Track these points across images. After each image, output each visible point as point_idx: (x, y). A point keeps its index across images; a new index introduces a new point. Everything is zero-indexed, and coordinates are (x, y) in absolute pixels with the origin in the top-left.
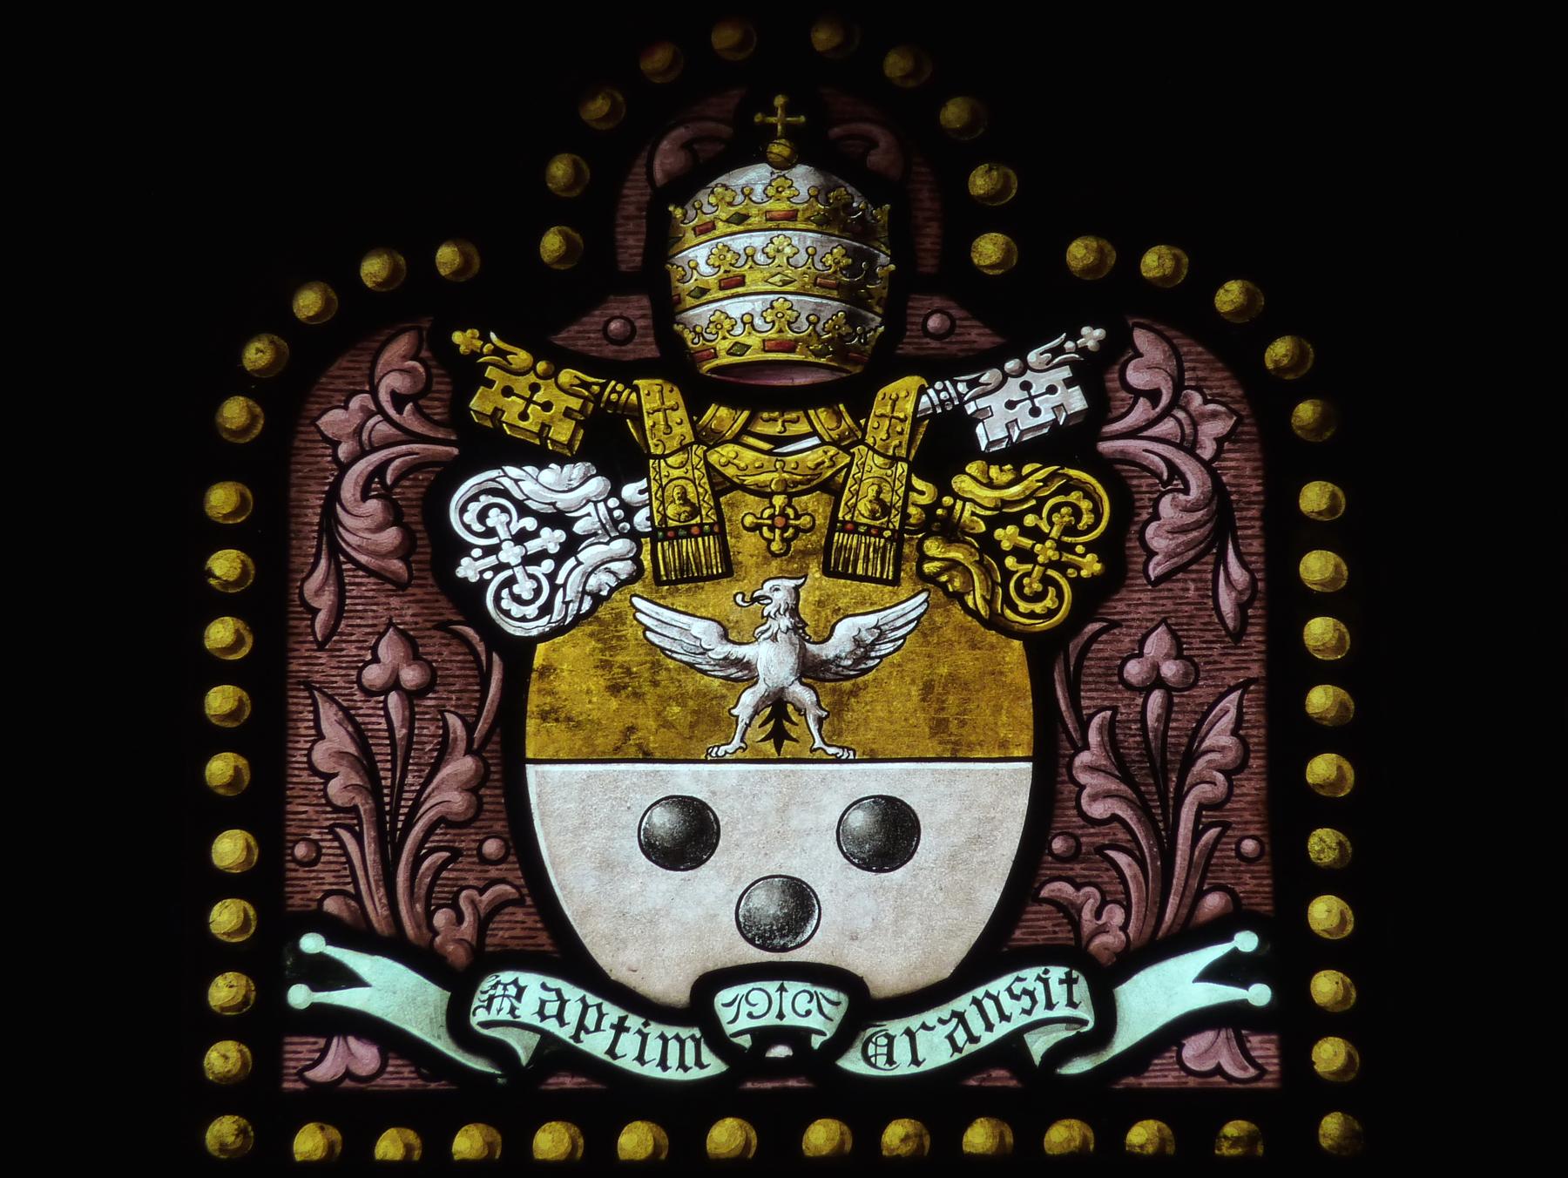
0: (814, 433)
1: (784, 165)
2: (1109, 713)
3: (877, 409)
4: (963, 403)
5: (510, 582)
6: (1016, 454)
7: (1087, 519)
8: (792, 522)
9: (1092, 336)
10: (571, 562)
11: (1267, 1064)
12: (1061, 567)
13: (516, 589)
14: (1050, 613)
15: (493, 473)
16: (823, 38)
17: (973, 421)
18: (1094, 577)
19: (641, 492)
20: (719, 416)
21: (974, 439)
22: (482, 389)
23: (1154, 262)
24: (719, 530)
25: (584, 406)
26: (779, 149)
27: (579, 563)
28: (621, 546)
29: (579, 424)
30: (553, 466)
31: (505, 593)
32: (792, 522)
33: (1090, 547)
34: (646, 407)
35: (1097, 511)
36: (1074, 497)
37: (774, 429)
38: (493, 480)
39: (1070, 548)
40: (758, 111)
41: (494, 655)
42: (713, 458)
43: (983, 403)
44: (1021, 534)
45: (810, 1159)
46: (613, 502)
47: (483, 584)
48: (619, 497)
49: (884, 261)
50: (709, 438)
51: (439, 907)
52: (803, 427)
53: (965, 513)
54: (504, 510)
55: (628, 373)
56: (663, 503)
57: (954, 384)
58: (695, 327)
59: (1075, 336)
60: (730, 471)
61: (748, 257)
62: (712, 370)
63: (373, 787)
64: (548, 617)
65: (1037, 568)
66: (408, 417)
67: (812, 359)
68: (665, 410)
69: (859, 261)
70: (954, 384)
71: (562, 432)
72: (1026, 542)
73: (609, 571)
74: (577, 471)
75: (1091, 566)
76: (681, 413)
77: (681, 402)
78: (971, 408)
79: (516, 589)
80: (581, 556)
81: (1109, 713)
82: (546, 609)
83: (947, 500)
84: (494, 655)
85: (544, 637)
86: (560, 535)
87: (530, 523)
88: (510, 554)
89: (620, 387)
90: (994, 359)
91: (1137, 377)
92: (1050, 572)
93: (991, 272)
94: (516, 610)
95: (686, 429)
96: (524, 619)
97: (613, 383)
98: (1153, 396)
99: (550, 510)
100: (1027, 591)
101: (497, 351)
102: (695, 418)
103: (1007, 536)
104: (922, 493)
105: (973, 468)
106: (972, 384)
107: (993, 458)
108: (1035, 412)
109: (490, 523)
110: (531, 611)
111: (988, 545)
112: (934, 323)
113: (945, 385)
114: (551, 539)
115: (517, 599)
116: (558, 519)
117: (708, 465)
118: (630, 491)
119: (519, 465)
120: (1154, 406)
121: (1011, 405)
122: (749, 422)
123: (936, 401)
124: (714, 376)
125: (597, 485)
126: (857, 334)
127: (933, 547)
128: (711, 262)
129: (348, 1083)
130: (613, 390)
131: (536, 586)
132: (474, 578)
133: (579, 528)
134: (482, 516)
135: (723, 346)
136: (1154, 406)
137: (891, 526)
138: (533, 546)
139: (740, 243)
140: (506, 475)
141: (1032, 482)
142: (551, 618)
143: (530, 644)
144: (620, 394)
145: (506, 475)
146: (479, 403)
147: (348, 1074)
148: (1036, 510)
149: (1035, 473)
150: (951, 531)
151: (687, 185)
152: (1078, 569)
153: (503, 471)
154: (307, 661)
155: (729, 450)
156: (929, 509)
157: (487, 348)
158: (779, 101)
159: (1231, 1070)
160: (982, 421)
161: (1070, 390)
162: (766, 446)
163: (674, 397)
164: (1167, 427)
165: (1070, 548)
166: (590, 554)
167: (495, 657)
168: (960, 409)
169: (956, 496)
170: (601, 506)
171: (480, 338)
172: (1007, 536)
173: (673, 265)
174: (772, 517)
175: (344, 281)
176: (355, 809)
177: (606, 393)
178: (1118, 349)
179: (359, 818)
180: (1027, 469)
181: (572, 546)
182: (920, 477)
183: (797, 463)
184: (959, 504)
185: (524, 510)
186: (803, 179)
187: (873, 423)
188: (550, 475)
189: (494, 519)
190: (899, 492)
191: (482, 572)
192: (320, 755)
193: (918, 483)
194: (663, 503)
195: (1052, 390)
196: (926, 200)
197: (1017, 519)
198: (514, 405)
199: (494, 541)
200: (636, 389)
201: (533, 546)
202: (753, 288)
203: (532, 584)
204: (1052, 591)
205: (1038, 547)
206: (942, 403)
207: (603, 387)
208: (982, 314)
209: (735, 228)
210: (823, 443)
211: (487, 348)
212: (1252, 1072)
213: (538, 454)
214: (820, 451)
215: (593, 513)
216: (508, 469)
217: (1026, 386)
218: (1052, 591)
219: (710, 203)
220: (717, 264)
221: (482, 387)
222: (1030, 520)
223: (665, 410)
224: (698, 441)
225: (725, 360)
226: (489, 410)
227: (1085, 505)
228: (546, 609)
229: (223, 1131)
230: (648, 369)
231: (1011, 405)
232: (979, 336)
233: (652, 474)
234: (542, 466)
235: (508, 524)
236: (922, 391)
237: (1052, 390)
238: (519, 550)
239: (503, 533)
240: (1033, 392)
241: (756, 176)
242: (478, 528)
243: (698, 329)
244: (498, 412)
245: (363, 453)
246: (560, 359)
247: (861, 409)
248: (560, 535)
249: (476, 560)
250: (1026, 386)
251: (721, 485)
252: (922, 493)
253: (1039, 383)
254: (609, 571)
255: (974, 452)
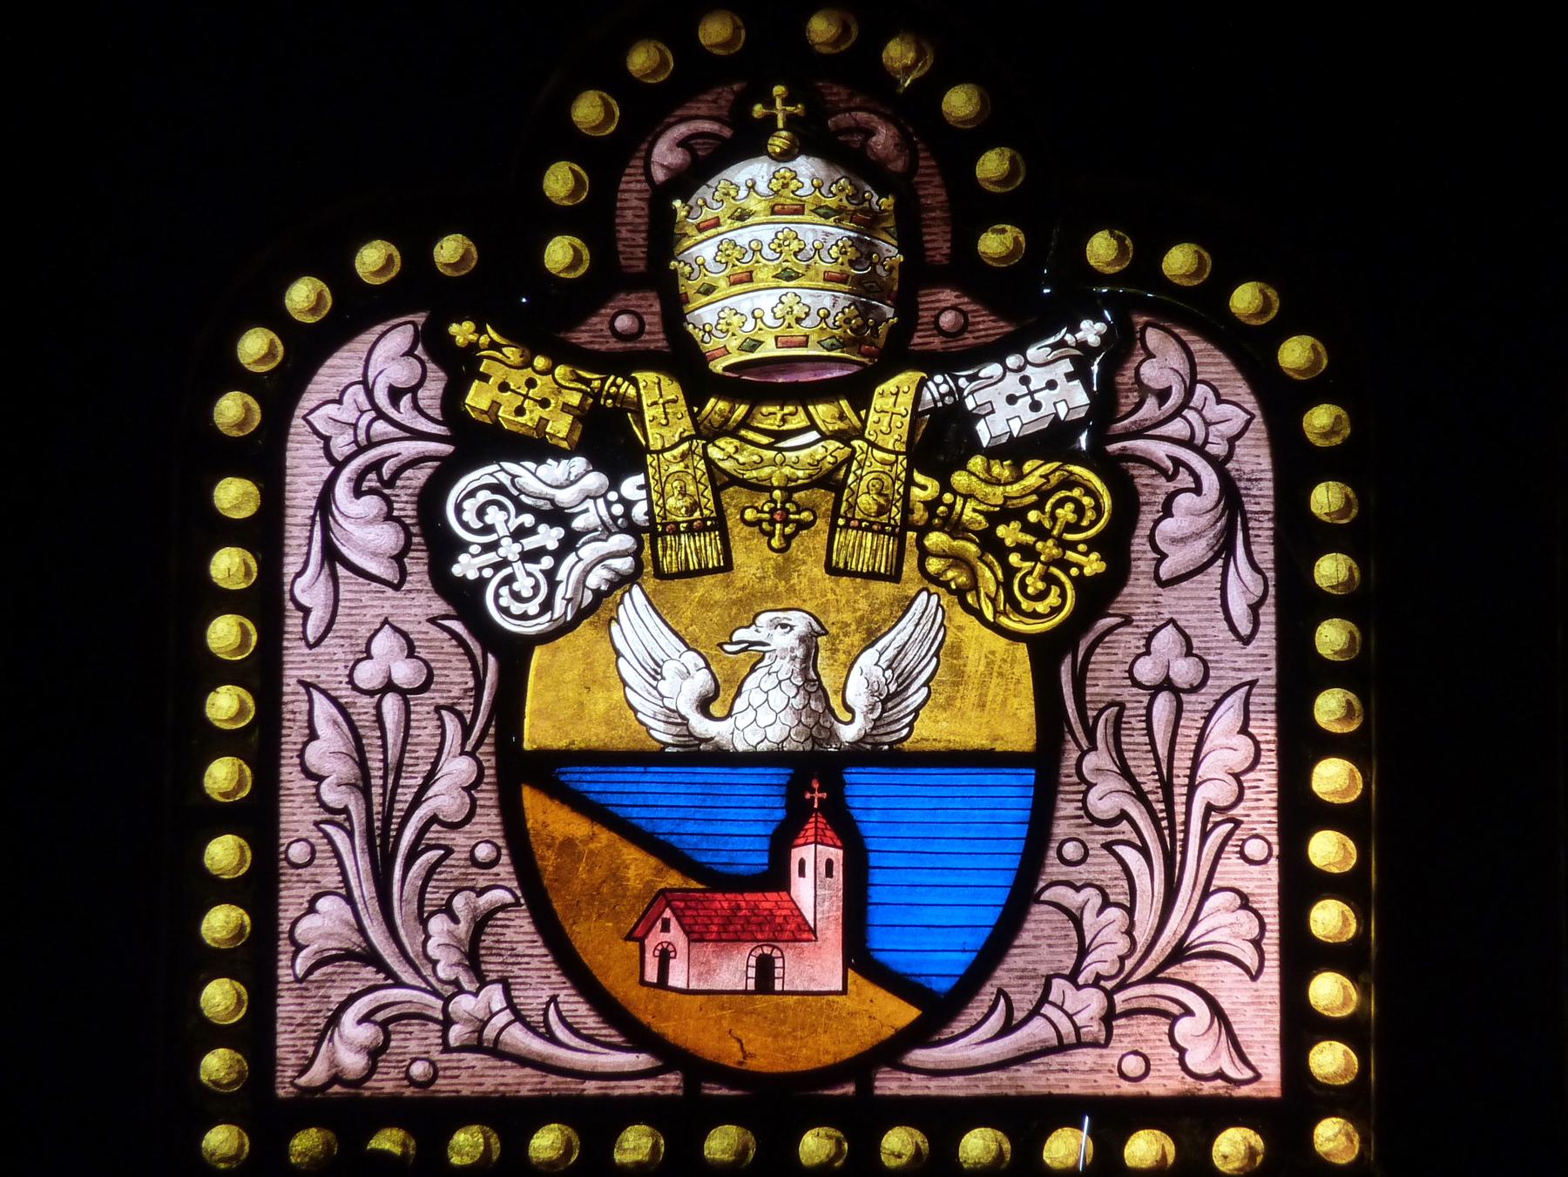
0: (813, 426)
1: (786, 156)
2: (1116, 709)
3: (877, 402)
4: (962, 399)
5: (509, 580)
6: (1015, 450)
7: (1090, 515)
8: (792, 516)
9: (1091, 331)
10: (572, 558)
11: (597, 1035)
12: (1065, 565)
13: (516, 586)
14: (1055, 611)
15: (494, 468)
16: (821, 28)
17: (975, 418)
18: (1097, 577)
19: (640, 487)
20: (715, 406)
21: (975, 438)
22: (476, 383)
23: (1179, 261)
24: (719, 524)
25: (583, 401)
26: (778, 142)
27: (580, 559)
28: (623, 541)
29: (577, 419)
30: (550, 461)
31: (504, 591)
32: (792, 516)
33: (1093, 545)
34: (645, 401)
35: (1098, 509)
36: (1076, 493)
37: (772, 424)
38: (491, 474)
39: (1073, 546)
40: (760, 102)
41: (490, 656)
42: (713, 452)
43: (982, 397)
44: (1022, 530)
45: (970, 1170)
46: (613, 496)
47: (482, 583)
48: (618, 491)
49: (890, 251)
50: (707, 432)
51: (432, 914)
52: (799, 421)
53: (970, 513)
54: (502, 507)
55: (625, 363)
56: (662, 495)
57: (955, 379)
58: (704, 326)
59: (1074, 329)
60: (727, 465)
61: (754, 251)
62: (726, 369)
63: (362, 786)
64: (549, 614)
65: (1039, 566)
66: (405, 414)
67: (826, 353)
68: (893, 414)
69: (863, 251)
70: (955, 379)
71: (560, 426)
72: (1029, 539)
73: (605, 567)
74: (579, 463)
75: (1093, 565)
76: (682, 406)
77: (681, 397)
78: (970, 404)
79: (516, 586)
80: (582, 553)
81: (1116, 709)
82: (547, 606)
83: (948, 497)
84: (490, 656)
85: (545, 638)
86: (559, 532)
87: (528, 520)
88: (510, 550)
89: (619, 380)
90: (996, 352)
91: (1151, 373)
92: (1055, 571)
93: (990, 263)
94: (517, 608)
95: (687, 423)
96: (524, 617)
97: (612, 378)
98: (1163, 395)
99: (548, 507)
100: (1030, 590)
101: (494, 345)
102: (696, 409)
103: (1009, 533)
104: (924, 488)
105: (977, 463)
106: (971, 379)
107: (993, 453)
108: (1035, 406)
109: (488, 520)
110: (533, 608)
111: (990, 544)
112: (947, 319)
113: (945, 378)
114: (549, 537)
115: (516, 596)
116: (557, 515)
117: (710, 463)
118: (631, 486)
119: (517, 460)
120: (1161, 405)
121: (1012, 400)
122: (748, 414)
123: (937, 395)
124: (731, 375)
125: (596, 480)
126: (868, 327)
127: (935, 539)
128: (718, 259)
129: (336, 1088)
130: (614, 384)
131: (533, 584)
132: (472, 575)
133: (578, 524)
134: (481, 512)
135: (733, 344)
136: (1161, 405)
137: (892, 522)
138: (530, 543)
139: (743, 237)
140: (503, 470)
141: (1033, 481)
142: (552, 614)
143: (531, 642)
144: (619, 387)
145: (503, 470)
146: (478, 398)
147: (336, 1078)
148: (1039, 506)
149: (1036, 472)
150: (955, 527)
151: (688, 180)
152: (1080, 567)
153: (500, 466)
154: (297, 664)
155: (728, 444)
156: (931, 506)
157: (484, 340)
158: (778, 90)
159: (1231, 1072)
160: (984, 416)
161: (1071, 383)
162: (765, 440)
163: (672, 390)
164: (1177, 428)
165: (1073, 546)
166: (588, 552)
167: (491, 659)
168: (960, 403)
169: (955, 493)
170: (601, 502)
171: (475, 332)
172: (1009, 533)
173: (679, 262)
174: (772, 511)
175: (340, 276)
176: (345, 810)
177: (606, 388)
178: (1121, 346)
179: (349, 819)
180: (1027, 467)
181: (570, 543)
182: (921, 472)
183: (797, 457)
184: (960, 501)
185: (522, 508)
186: (806, 168)
187: (873, 417)
188: (553, 470)
189: (494, 516)
190: (703, 481)
191: (480, 569)
192: (314, 755)
193: (919, 478)
194: (662, 495)
195: (1051, 385)
196: (933, 193)
197: (1019, 514)
198: (508, 402)
199: (492, 538)
200: (634, 382)
201: (530, 543)
202: (761, 285)
203: (531, 581)
204: (1055, 590)
205: (1039, 545)
206: (942, 396)
207: (604, 381)
208: (997, 308)
209: (738, 224)
210: (824, 437)
211: (484, 340)
212: (1248, 1074)
213: (536, 448)
214: (818, 447)
215: (592, 509)
216: (506, 465)
217: (1025, 381)
218: (1055, 590)
219: (711, 199)
220: (723, 261)
221: (477, 381)
222: (1033, 516)
223: (893, 414)
224: (698, 436)
225: (736, 358)
226: (484, 405)
227: (1087, 501)
228: (547, 606)
229: (220, 1139)
230: (650, 361)
231: (1012, 400)
232: (988, 327)
233: (651, 470)
234: (540, 460)
235: (507, 522)
236: (922, 384)
237: (1051, 385)
238: (517, 548)
239: (502, 530)
240: (1032, 387)
241: (755, 172)
242: (477, 525)
243: (707, 328)
244: (495, 405)
245: (361, 450)
246: (562, 353)
247: (862, 401)
248: (559, 532)
249: (474, 556)
250: (1025, 381)
251: (720, 479)
252: (924, 488)
253: (1038, 378)
254: (608, 568)
255: (974, 446)
